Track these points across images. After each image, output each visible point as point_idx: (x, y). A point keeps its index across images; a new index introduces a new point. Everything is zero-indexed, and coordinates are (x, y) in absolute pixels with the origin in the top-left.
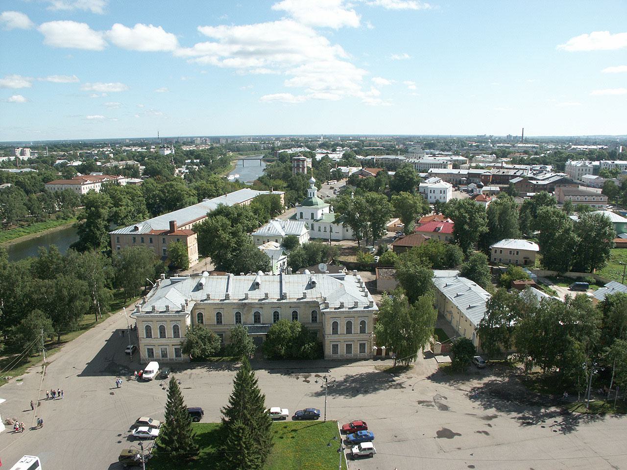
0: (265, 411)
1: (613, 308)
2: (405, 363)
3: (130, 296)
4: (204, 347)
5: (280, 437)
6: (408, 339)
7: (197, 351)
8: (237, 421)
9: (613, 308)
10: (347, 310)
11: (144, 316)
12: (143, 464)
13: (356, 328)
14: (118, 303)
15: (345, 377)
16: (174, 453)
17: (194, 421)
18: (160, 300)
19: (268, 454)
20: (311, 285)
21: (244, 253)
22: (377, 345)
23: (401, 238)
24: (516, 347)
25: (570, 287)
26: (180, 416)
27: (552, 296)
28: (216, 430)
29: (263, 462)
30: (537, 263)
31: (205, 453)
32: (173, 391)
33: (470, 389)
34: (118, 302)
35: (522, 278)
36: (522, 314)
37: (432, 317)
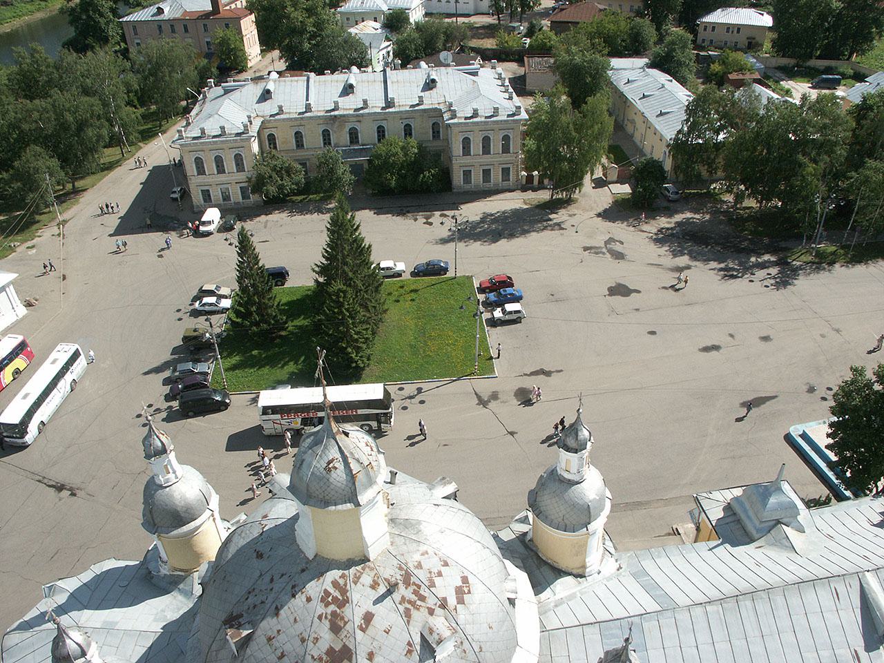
0: (372, 267)
1: (871, 115)
2: (566, 195)
3: (167, 116)
4: (280, 182)
5: (395, 301)
6: (571, 161)
7: (272, 190)
8: (335, 282)
9: (871, 115)
10: (483, 119)
11: (190, 144)
12: (214, 346)
13: (496, 146)
14: (151, 128)
15: (481, 216)
16: (254, 328)
17: (276, 285)
18: (211, 119)
19: (380, 323)
20: (430, 85)
21: (329, 41)
22: (526, 169)
23: (562, 10)
24: (724, 171)
25: (812, 84)
26: (257, 281)
27: (783, 97)
28: (307, 295)
29: (374, 333)
30: (767, 45)
31: (296, 326)
32: (245, 246)
33: (656, 230)
34: (149, 126)
35: (741, 70)
36: (736, 124)
37: (607, 128)
